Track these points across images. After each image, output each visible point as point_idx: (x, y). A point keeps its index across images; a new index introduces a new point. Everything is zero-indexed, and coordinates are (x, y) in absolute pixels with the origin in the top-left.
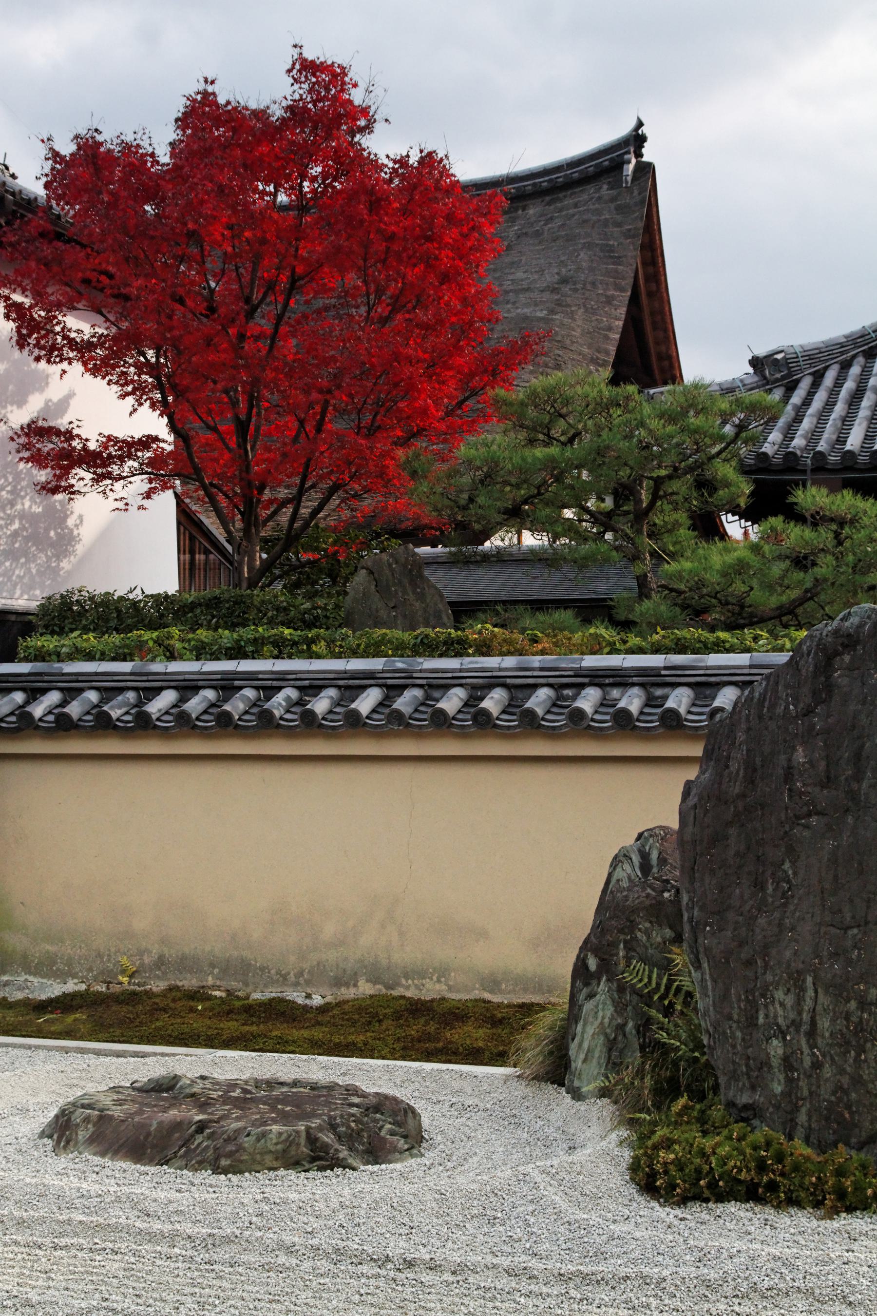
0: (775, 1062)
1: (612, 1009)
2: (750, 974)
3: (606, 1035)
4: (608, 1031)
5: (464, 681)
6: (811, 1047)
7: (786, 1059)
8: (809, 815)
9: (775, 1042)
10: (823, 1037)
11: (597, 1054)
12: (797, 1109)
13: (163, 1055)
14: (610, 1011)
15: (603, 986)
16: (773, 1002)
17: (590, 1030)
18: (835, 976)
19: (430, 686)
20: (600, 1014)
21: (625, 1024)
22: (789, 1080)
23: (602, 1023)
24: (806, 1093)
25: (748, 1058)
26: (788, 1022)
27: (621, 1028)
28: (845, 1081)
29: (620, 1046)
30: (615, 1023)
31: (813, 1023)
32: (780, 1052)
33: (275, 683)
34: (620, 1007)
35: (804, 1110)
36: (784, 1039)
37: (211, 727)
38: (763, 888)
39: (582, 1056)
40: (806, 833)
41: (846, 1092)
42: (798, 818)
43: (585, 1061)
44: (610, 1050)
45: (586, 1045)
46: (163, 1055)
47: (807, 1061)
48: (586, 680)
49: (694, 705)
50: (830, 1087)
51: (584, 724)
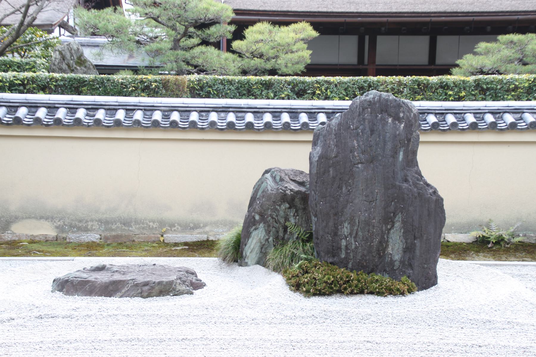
0: (343, 247)
1: (265, 233)
2: (336, 218)
3: (261, 243)
4: (262, 241)
5: (160, 108)
6: (355, 241)
7: (346, 246)
8: (358, 163)
9: (343, 241)
10: (360, 238)
11: (256, 250)
12: (348, 263)
13: (60, 260)
14: (264, 233)
15: (262, 225)
16: (343, 227)
17: (254, 241)
18: (366, 218)
19: (145, 110)
20: (260, 235)
21: (269, 238)
22: (347, 253)
23: (260, 239)
24: (352, 257)
25: (333, 246)
26: (348, 233)
27: (267, 240)
28: (365, 252)
29: (266, 246)
30: (265, 238)
31: (357, 234)
32: (345, 244)
33: (75, 106)
34: (268, 232)
35: (351, 263)
36: (346, 239)
37: (261, 129)
38: (341, 189)
39: (250, 251)
40: (357, 170)
41: (365, 256)
42: (355, 164)
43: (251, 252)
44: (262, 248)
45: (252, 247)
46: (60, 260)
47: (353, 246)
48: (211, 109)
49: (47, 115)
50: (360, 254)
51: (215, 127)
